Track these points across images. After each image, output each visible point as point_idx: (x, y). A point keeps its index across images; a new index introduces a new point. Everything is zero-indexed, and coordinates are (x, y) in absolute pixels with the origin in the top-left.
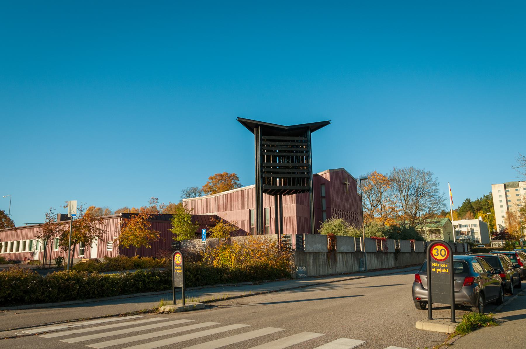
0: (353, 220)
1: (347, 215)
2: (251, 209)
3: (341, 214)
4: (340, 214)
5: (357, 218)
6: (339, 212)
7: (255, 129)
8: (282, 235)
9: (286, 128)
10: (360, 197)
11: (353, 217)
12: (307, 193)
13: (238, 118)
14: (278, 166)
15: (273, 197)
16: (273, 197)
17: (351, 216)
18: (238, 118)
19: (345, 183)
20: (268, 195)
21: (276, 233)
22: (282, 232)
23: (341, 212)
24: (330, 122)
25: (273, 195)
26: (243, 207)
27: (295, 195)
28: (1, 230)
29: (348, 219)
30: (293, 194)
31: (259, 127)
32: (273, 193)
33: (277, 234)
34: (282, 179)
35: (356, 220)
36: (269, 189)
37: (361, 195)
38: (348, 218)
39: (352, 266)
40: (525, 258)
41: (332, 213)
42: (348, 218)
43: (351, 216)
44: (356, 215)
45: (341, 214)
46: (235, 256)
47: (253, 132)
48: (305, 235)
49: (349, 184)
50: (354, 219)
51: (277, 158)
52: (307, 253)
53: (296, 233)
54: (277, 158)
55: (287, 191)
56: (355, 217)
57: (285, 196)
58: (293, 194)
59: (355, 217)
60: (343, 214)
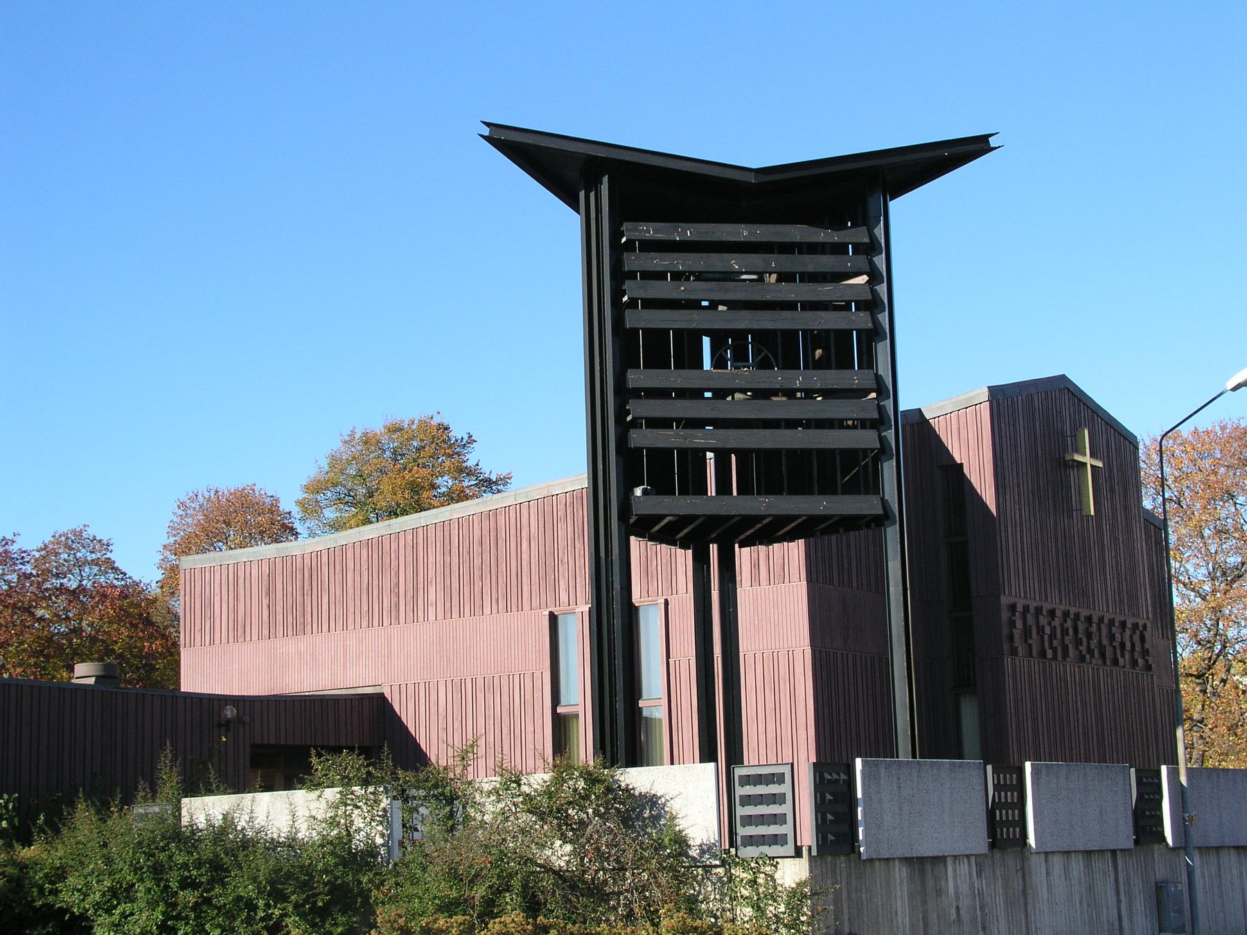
0: (1121, 660)
1: (1089, 636)
2: (556, 611)
3: (1053, 630)
4: (1048, 630)
5: (1145, 653)
6: (1043, 620)
7: (582, 194)
8: (739, 772)
9: (752, 179)
10: (1156, 529)
11: (1123, 645)
12: (870, 531)
13: (488, 124)
14: (708, 390)
15: (684, 558)
16: (684, 558)
17: (1112, 637)
18: (488, 124)
19: (1078, 458)
20: (650, 543)
21: (703, 759)
22: (735, 756)
23: (1057, 622)
24: (993, 142)
25: (684, 546)
26: (512, 601)
27: (802, 542)
28: (922, 932)
29: (1092, 656)
30: (790, 537)
31: (606, 179)
32: (681, 534)
33: (712, 765)
34: (733, 455)
35: (1134, 663)
36: (664, 516)
37: (1165, 520)
38: (1091, 652)
39: (1117, 925)
40: (253, 933)
41: (1005, 631)
42: (1091, 652)
43: (1112, 637)
44: (1136, 638)
45: (1053, 630)
46: (180, 851)
47: (574, 205)
48: (864, 764)
49: (1100, 464)
50: (1127, 655)
51: (706, 341)
52: (915, 860)
53: (815, 761)
54: (706, 341)
55: (758, 526)
56: (1133, 645)
57: (746, 550)
58: (792, 540)
59: (1133, 645)
60: (1065, 632)
